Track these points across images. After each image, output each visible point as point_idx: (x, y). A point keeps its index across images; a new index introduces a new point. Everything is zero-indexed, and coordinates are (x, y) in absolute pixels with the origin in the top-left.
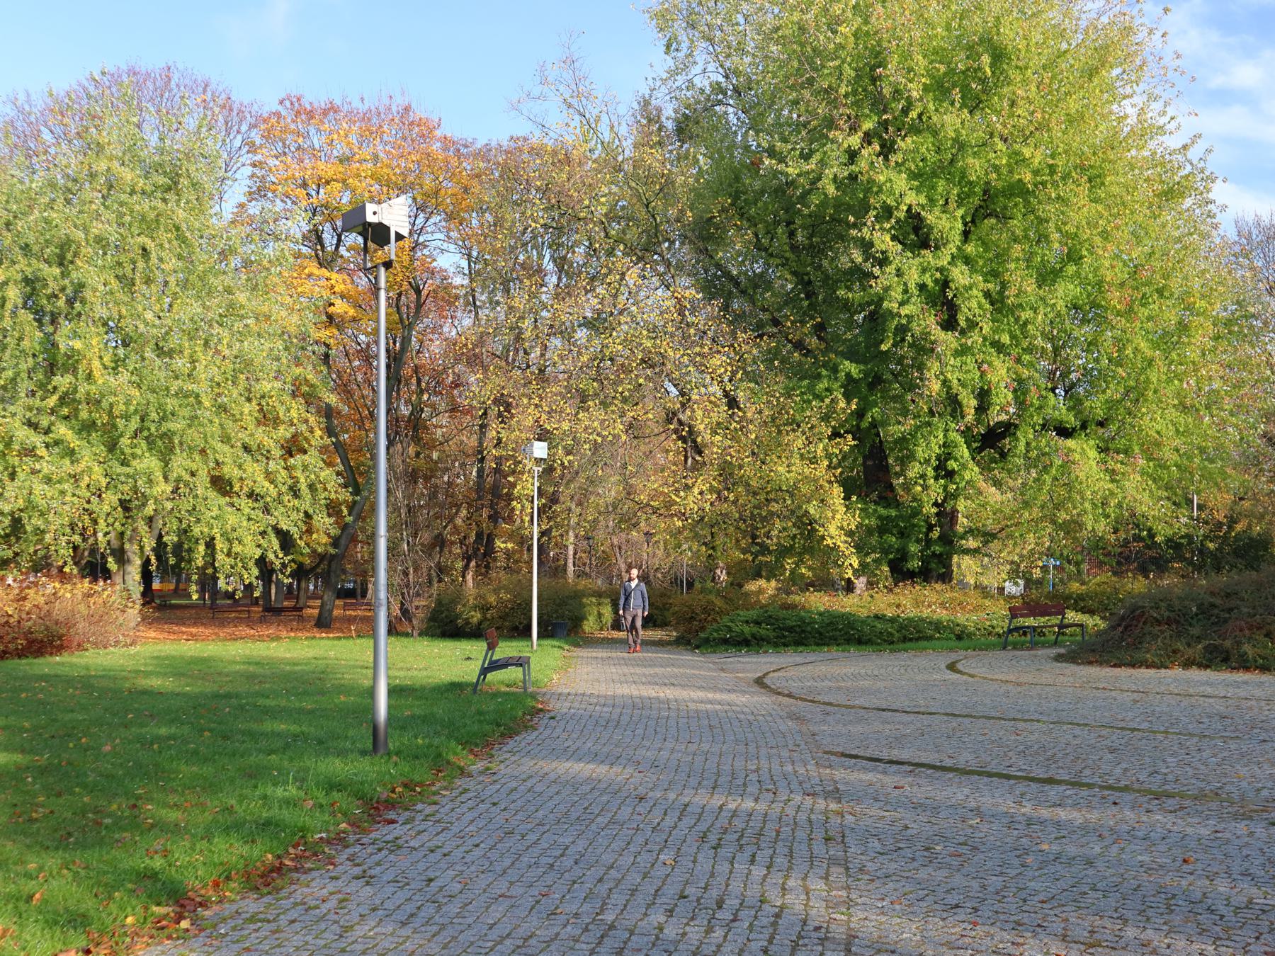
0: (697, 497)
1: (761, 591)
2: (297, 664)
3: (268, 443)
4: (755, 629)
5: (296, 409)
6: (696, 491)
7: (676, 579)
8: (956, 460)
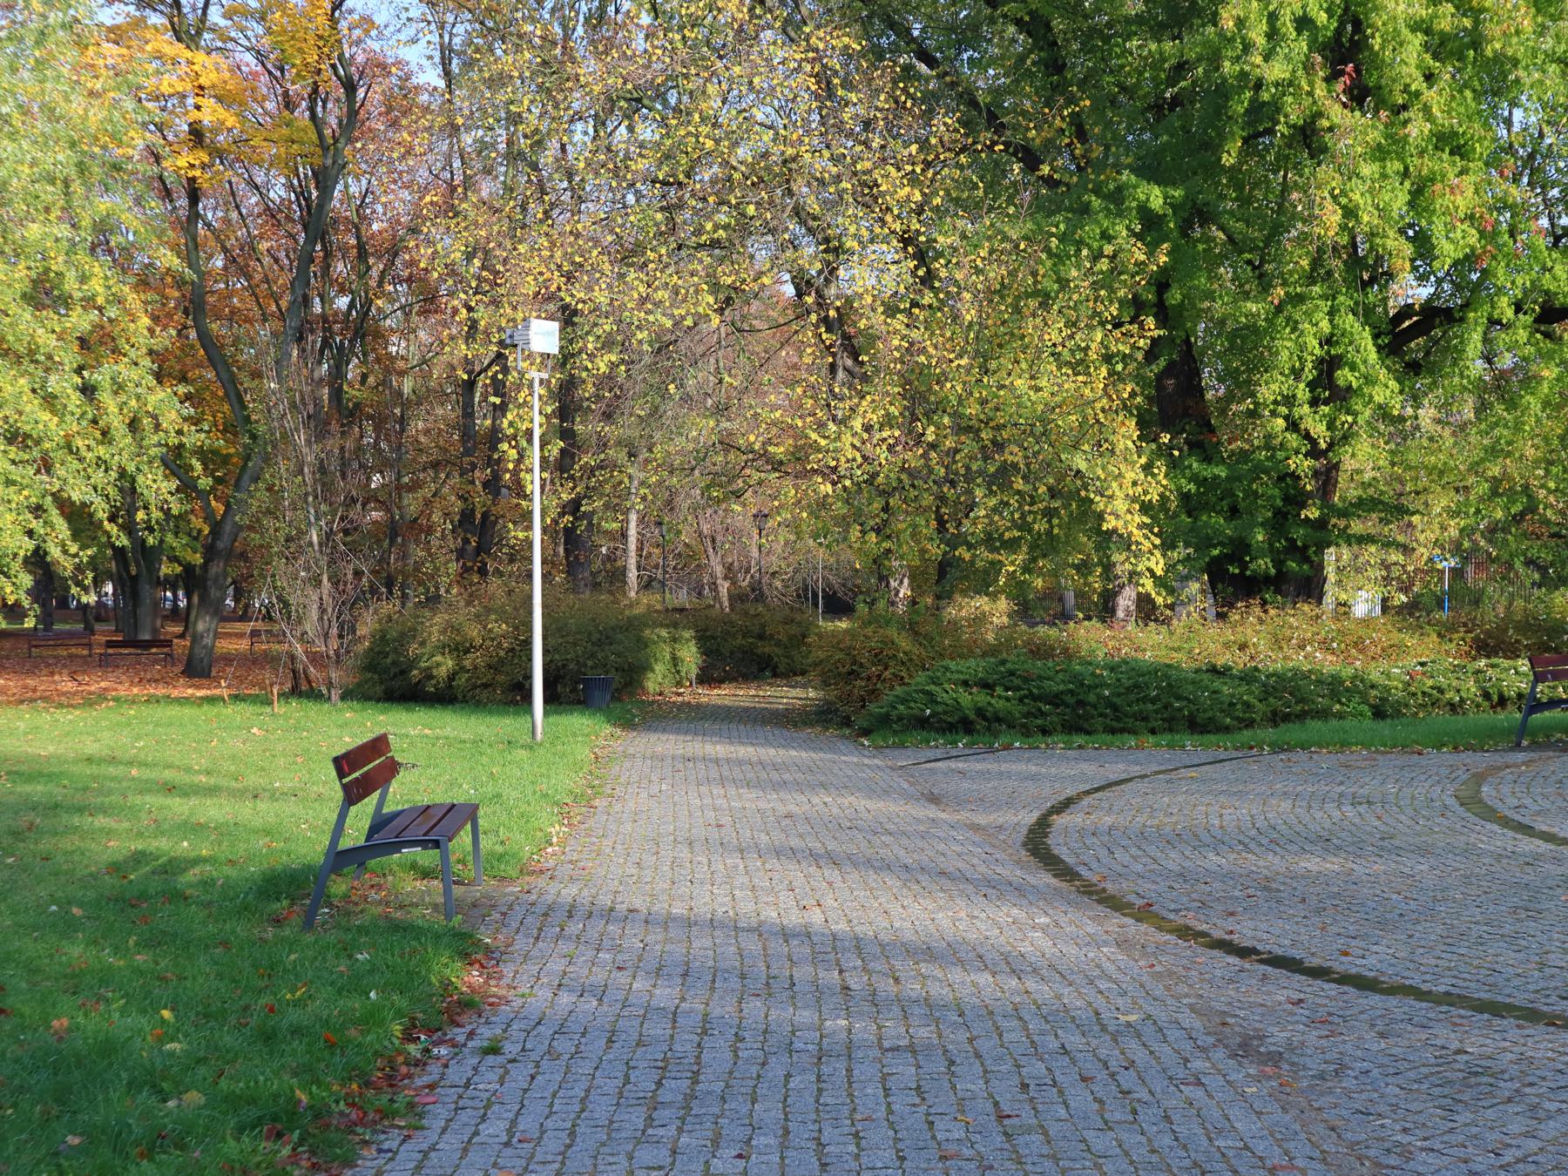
0: (861, 435)
1: (980, 619)
2: (30, 778)
3: (47, 341)
4: (982, 698)
5: (100, 279)
6: (857, 424)
7: (806, 589)
8: (1353, 368)
